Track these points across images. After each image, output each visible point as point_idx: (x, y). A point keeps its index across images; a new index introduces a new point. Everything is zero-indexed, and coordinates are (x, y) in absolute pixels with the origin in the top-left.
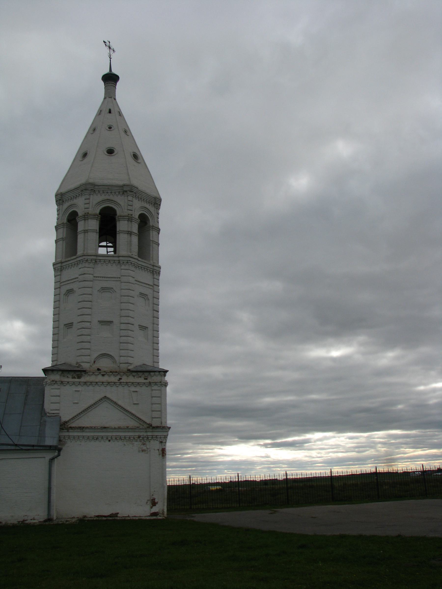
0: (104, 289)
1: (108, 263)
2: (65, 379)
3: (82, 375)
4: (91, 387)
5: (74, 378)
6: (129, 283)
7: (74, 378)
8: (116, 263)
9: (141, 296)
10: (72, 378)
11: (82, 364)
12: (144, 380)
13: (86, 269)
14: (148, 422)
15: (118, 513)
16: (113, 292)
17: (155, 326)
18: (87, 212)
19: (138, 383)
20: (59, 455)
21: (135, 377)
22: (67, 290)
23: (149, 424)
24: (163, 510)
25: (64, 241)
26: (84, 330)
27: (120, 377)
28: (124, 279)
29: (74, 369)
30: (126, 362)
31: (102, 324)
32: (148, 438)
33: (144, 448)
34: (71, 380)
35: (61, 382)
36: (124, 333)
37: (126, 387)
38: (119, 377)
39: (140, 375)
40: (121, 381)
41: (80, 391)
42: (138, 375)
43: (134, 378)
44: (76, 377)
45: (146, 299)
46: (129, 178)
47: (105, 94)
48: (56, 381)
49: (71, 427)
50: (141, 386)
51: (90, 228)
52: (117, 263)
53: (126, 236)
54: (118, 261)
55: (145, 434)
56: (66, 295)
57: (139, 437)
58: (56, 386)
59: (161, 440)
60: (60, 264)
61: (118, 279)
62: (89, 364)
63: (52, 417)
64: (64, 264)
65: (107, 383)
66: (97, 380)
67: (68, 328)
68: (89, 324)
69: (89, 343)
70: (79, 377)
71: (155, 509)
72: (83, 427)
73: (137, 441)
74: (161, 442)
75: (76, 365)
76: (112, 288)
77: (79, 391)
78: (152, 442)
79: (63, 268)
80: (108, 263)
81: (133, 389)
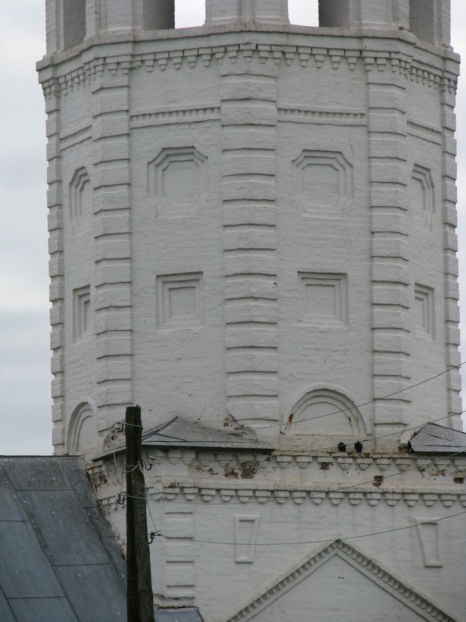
1: (322, 58)
3: (257, 463)
5: (231, 474)
6: (396, 133)
7: (233, 474)
8: (350, 60)
9: (416, 175)
10: (226, 475)
11: (254, 425)
12: (453, 482)
13: (252, 80)
16: (342, 166)
17: (450, 279)
19: (439, 495)
21: (426, 473)
22: (164, 149)
26: (253, 303)
27: (378, 474)
29: (229, 445)
30: (396, 420)
31: (311, 282)
35: (196, 491)
37: (401, 507)
38: (374, 472)
39: (441, 468)
40: (385, 486)
41: (256, 522)
42: (436, 465)
43: (423, 477)
44: (236, 471)
45: (426, 186)
48: (181, 485)
50: (448, 507)
52: (354, 60)
54: (358, 54)
56: (157, 166)
60: (130, 45)
61: (358, 120)
63: (171, 611)
65: (341, 495)
66: (309, 485)
67: (171, 289)
68: (271, 281)
69: (272, 353)
75: (222, 428)
76: (340, 153)
77: (253, 521)
79: (139, 64)
80: (322, 58)
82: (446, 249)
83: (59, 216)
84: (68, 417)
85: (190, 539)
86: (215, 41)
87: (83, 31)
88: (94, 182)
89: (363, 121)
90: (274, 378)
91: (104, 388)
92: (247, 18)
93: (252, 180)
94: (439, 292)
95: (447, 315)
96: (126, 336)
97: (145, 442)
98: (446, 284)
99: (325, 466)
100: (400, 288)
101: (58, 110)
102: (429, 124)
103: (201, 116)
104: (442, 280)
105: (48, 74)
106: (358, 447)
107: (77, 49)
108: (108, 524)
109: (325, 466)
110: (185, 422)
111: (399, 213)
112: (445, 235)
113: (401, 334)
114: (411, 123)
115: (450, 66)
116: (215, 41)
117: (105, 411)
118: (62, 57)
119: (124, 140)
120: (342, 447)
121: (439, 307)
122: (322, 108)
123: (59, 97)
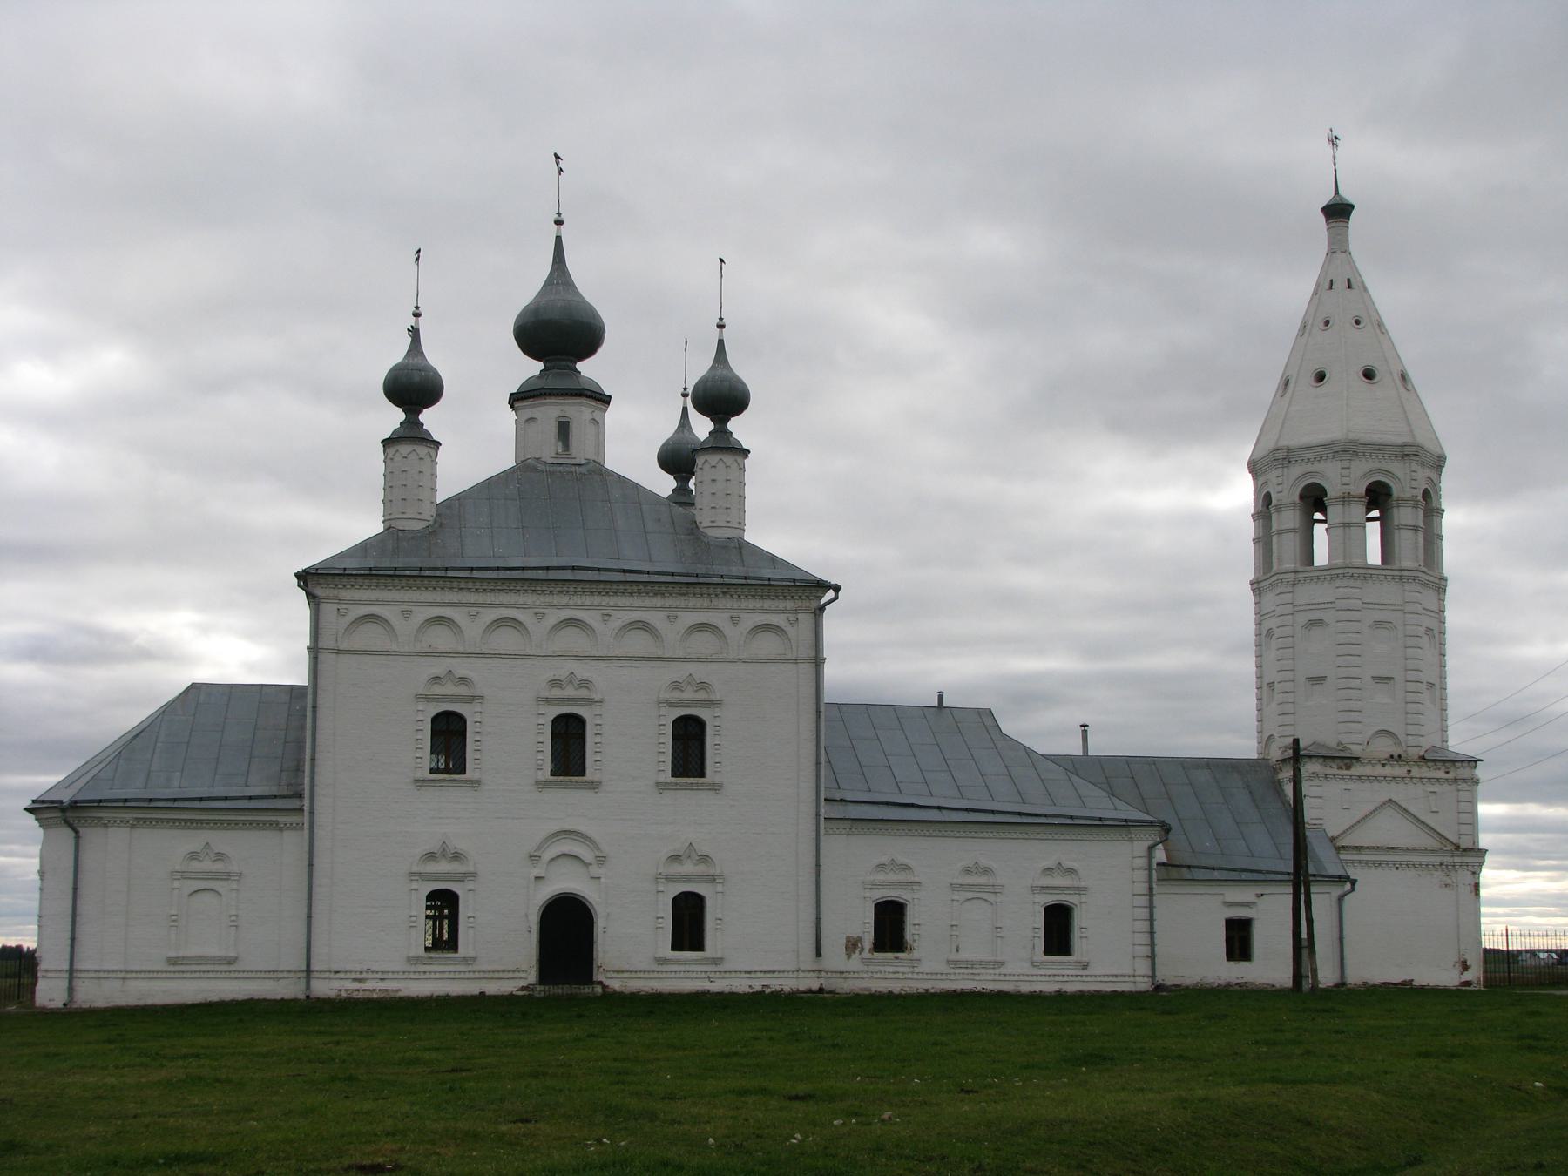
0: (1378, 624)
2: (1329, 771)
4: (1367, 785)
11: (1351, 746)
14: (1454, 842)
15: (1412, 980)
18: (1347, 491)
19: (1438, 779)
20: (1353, 889)
23: (1455, 845)
24: (1479, 978)
25: (1297, 534)
28: (1409, 607)
32: (1454, 866)
33: (1448, 881)
34: (1335, 771)
36: (1411, 697)
37: (1419, 784)
40: (1411, 774)
46: (1411, 431)
47: (1330, 243)
49: (1343, 847)
51: (1355, 521)
53: (1410, 534)
55: (1451, 860)
57: (1441, 864)
58: (1316, 782)
59: (1473, 870)
61: (1400, 608)
62: (1361, 747)
64: (1300, 575)
66: (1376, 774)
68: (1359, 681)
69: (1360, 713)
70: (1348, 768)
71: (1468, 976)
72: (1362, 847)
73: (1437, 870)
74: (1474, 873)
78: (1460, 871)
81: (1430, 788)
82: (1441, 666)
83: (1261, 650)
84: (1264, 742)
85: (1320, 797)
86: (1333, 572)
87: (1272, 568)
88: (1276, 636)
89: (1402, 608)
90: (1360, 725)
91: (1281, 728)
92: (1348, 562)
93: (1350, 635)
94: (1437, 686)
95: (1441, 695)
96: (1291, 705)
97: (1302, 753)
98: (1441, 682)
99: (1384, 765)
100: (1419, 684)
101: (1260, 602)
102: (1432, 608)
103: (1326, 606)
104: (1438, 680)
105: (1255, 586)
106: (1400, 756)
107: (1269, 575)
108: (1283, 790)
109: (1384, 765)
110: (1319, 744)
111: (1419, 650)
112: (1440, 660)
113: (1419, 705)
114: (1424, 609)
115: (1443, 582)
116: (1333, 572)
117: (1282, 739)
118: (1262, 579)
119: (1290, 617)
120: (1392, 757)
121: (1438, 693)
122: (1382, 602)
123: (1260, 597)
